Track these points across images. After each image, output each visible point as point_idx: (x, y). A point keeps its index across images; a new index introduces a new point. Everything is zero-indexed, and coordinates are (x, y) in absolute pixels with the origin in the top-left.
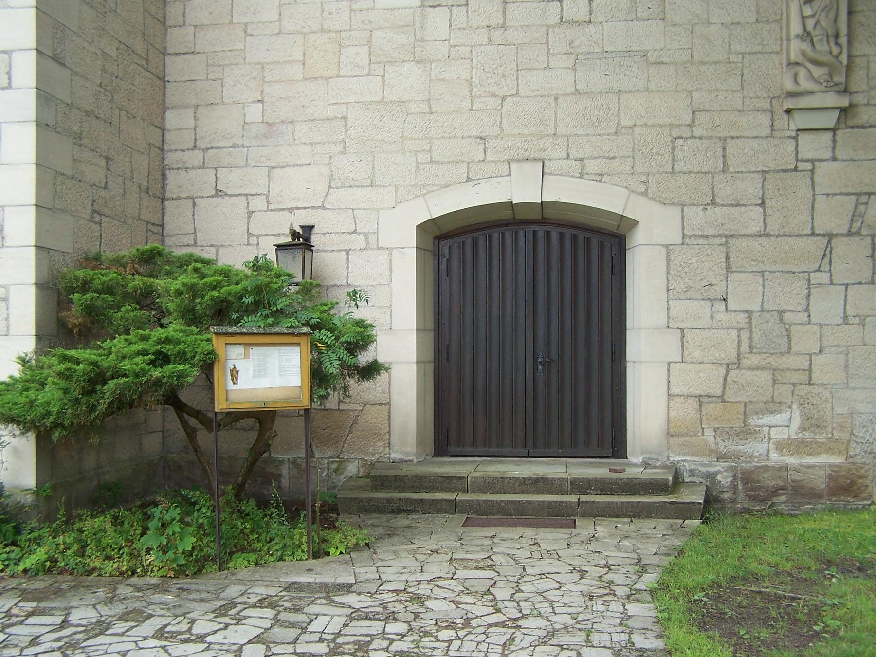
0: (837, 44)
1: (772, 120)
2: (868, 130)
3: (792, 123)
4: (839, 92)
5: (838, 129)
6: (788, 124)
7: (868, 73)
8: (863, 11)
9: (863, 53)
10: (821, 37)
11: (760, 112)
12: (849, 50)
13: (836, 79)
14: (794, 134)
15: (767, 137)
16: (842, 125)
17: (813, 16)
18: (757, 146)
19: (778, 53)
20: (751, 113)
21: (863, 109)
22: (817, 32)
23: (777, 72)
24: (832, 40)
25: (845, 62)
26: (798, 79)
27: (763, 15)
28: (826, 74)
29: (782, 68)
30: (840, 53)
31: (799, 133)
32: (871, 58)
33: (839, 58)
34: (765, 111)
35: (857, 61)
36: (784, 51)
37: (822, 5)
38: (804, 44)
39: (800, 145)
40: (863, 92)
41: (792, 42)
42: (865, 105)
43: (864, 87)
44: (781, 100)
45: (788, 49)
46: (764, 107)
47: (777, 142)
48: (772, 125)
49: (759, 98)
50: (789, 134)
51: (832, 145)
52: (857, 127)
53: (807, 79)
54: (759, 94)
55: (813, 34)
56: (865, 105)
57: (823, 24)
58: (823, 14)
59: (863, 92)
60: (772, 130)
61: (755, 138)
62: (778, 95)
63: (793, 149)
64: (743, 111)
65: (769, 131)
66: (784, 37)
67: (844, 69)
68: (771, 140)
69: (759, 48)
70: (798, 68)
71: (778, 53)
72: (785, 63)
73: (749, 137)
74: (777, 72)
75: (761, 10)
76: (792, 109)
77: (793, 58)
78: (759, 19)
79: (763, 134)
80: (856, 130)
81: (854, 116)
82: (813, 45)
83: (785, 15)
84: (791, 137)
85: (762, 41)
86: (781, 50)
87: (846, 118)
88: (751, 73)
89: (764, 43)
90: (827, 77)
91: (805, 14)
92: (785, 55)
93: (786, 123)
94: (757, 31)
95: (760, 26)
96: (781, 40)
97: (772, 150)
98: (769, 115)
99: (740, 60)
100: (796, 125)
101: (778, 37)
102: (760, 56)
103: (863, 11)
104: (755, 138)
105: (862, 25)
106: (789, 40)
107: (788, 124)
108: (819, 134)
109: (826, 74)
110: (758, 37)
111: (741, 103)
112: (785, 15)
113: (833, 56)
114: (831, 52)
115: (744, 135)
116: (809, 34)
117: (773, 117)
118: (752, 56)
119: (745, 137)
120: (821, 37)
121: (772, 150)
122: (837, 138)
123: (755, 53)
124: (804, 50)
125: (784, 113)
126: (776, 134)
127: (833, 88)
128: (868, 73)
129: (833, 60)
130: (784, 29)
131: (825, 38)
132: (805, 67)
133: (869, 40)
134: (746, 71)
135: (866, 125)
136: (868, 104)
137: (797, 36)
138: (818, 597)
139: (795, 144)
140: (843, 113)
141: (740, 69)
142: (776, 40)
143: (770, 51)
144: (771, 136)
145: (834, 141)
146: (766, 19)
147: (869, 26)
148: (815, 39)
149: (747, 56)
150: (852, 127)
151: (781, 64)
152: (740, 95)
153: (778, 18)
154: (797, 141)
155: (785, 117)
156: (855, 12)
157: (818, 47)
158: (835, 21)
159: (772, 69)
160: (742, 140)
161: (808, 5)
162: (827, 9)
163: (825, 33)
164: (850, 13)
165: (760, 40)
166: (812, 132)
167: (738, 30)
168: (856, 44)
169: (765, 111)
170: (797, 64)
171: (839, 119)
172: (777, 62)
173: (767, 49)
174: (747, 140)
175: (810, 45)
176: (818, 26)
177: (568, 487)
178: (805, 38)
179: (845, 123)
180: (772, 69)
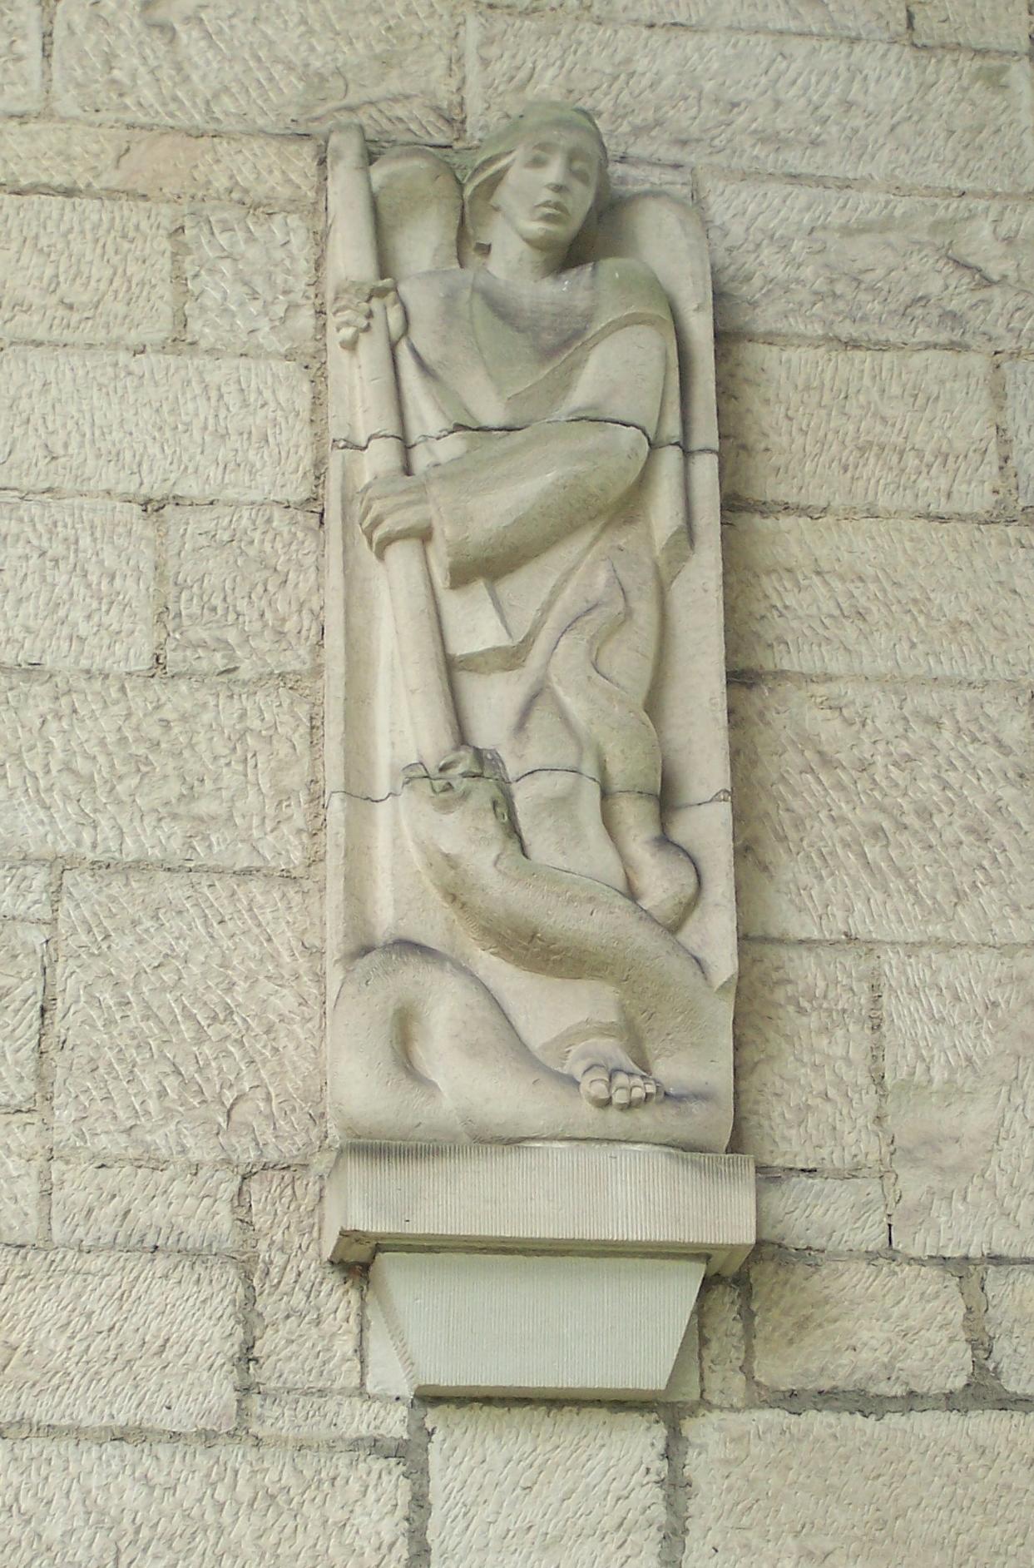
0: (664, 841)
1: (248, 1313)
2: (894, 1420)
3: (380, 1348)
4: (686, 1148)
5: (704, 1403)
6: (361, 1351)
7: (876, 1053)
8: (828, 678)
9: (837, 925)
10: (562, 782)
11: (161, 1264)
12: (742, 894)
13: (672, 1069)
14: (395, 1424)
15: (208, 1437)
16: (727, 1382)
17: (511, 658)
18: (134, 1495)
19: (288, 877)
20: (95, 1263)
21: (856, 1279)
22: (535, 755)
23: (285, 1001)
24: (636, 818)
25: (724, 963)
26: (419, 1051)
27: (200, 633)
28: (605, 1031)
29: (320, 978)
30: (692, 903)
31: (432, 1417)
32: (890, 960)
33: (690, 936)
34: (196, 1255)
35: (806, 969)
36: (334, 862)
37: (569, 599)
38: (451, 819)
39: (436, 1496)
40: (853, 1173)
41: (382, 812)
42: (871, 1257)
43: (865, 1145)
44: (308, 1189)
45: (357, 853)
46: (194, 1233)
47: (277, 1472)
48: (247, 1356)
49: (159, 1166)
50: (359, 1420)
51: (659, 1512)
52: (827, 1398)
53: (474, 1051)
54: (160, 1139)
55: (512, 768)
56: (871, 1257)
57: (576, 706)
58: (572, 650)
59: (853, 1173)
60: (245, 1390)
61: (121, 1436)
62: (288, 1150)
63: (391, 1528)
64: (45, 1245)
65: (221, 1392)
66: (333, 778)
67: (725, 1011)
68: (236, 1456)
69: (169, 839)
70: (412, 975)
71: (288, 877)
72: (335, 943)
73: (77, 1433)
74: (285, 1001)
75: (188, 606)
76: (381, 1245)
77: (386, 918)
78: (171, 656)
79: (184, 1417)
80: (819, 1421)
81: (802, 1325)
82: (512, 830)
83: (335, 641)
84: (376, 1446)
85: (189, 796)
86: (315, 860)
87: (749, 1333)
88: (109, 999)
89: (204, 807)
90: (612, 1049)
91: (461, 646)
92: (335, 889)
93: (345, 1345)
94: (156, 732)
95: (178, 698)
96: (317, 798)
97: (243, 1529)
98: (224, 1288)
99: (34, 902)
100: (409, 1362)
101: (294, 778)
102: (173, 889)
103: (828, 678)
104: (121, 1436)
105: (826, 760)
106: (359, 796)
107: (361, 1351)
108: (568, 1429)
109: (605, 1031)
110: (163, 764)
111: (30, 1187)
112: (335, 641)
113: (647, 916)
114: (631, 894)
115: (42, 1410)
116: (485, 763)
117: (251, 1299)
118: (116, 887)
119: (51, 1431)
120: (562, 782)
121: (243, 1529)
122: (695, 1465)
123: (140, 866)
124: (451, 861)
125: (334, 1279)
126: (275, 1420)
127: (645, 1119)
128: (876, 1053)
129: (644, 938)
130: (333, 729)
131: (590, 795)
132: (464, 970)
133: (873, 851)
134: (70, 981)
135: (884, 1388)
136: (889, 1254)
137: (413, 774)
138: (580, 43)
139: (404, 1497)
140: (726, 1302)
141: (29, 965)
142: (283, 796)
143: (242, 863)
144: (240, 1431)
145: (676, 1487)
146: (220, 661)
147: (864, 767)
148: (523, 797)
149: (80, 884)
150: (791, 1400)
151: (315, 953)
152: (25, 1136)
153: (296, 659)
154: (418, 1473)
155: (338, 1299)
156: (781, 675)
157: (542, 843)
158: (654, 705)
159: (252, 979)
160: (26, 1450)
161: (479, 587)
162: (597, 619)
163: (589, 767)
164: (740, 679)
165: (174, 789)
166: (518, 1413)
167: (31, 716)
168: (791, 869)
169: (196, 1255)
170: (407, 947)
171: (701, 1311)
172: (284, 940)
173: (221, 848)
174: (66, 1446)
175: (490, 825)
176: (541, 719)
177: (319, 661)
178: (460, 785)
179: (746, 1370)
180: (252, 979)
